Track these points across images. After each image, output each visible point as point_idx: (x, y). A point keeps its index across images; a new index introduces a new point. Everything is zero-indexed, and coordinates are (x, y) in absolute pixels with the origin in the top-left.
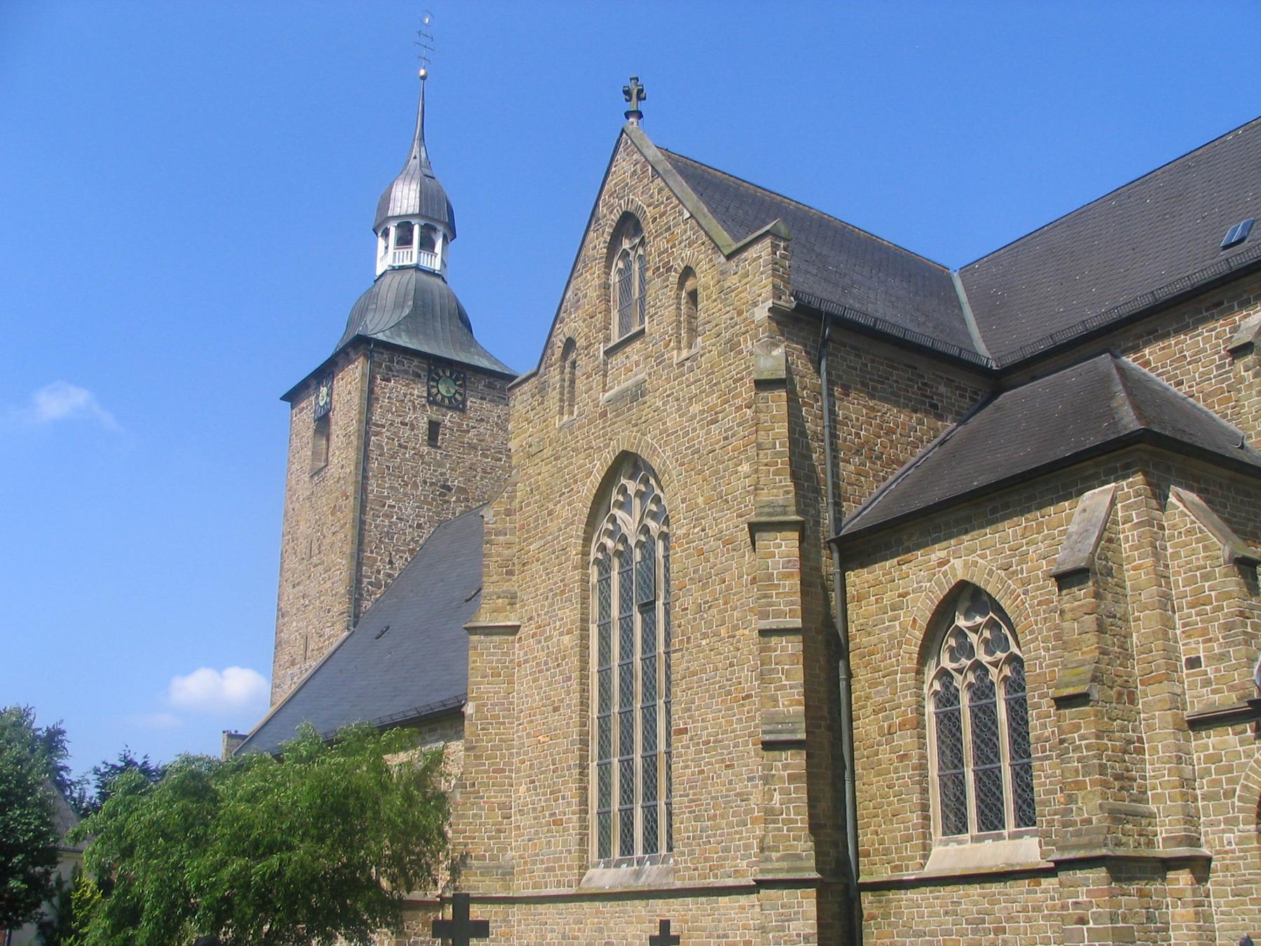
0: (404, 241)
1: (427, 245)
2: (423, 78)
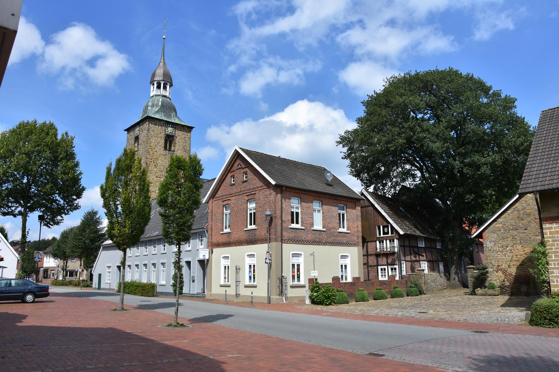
0: (159, 87)
1: (165, 88)
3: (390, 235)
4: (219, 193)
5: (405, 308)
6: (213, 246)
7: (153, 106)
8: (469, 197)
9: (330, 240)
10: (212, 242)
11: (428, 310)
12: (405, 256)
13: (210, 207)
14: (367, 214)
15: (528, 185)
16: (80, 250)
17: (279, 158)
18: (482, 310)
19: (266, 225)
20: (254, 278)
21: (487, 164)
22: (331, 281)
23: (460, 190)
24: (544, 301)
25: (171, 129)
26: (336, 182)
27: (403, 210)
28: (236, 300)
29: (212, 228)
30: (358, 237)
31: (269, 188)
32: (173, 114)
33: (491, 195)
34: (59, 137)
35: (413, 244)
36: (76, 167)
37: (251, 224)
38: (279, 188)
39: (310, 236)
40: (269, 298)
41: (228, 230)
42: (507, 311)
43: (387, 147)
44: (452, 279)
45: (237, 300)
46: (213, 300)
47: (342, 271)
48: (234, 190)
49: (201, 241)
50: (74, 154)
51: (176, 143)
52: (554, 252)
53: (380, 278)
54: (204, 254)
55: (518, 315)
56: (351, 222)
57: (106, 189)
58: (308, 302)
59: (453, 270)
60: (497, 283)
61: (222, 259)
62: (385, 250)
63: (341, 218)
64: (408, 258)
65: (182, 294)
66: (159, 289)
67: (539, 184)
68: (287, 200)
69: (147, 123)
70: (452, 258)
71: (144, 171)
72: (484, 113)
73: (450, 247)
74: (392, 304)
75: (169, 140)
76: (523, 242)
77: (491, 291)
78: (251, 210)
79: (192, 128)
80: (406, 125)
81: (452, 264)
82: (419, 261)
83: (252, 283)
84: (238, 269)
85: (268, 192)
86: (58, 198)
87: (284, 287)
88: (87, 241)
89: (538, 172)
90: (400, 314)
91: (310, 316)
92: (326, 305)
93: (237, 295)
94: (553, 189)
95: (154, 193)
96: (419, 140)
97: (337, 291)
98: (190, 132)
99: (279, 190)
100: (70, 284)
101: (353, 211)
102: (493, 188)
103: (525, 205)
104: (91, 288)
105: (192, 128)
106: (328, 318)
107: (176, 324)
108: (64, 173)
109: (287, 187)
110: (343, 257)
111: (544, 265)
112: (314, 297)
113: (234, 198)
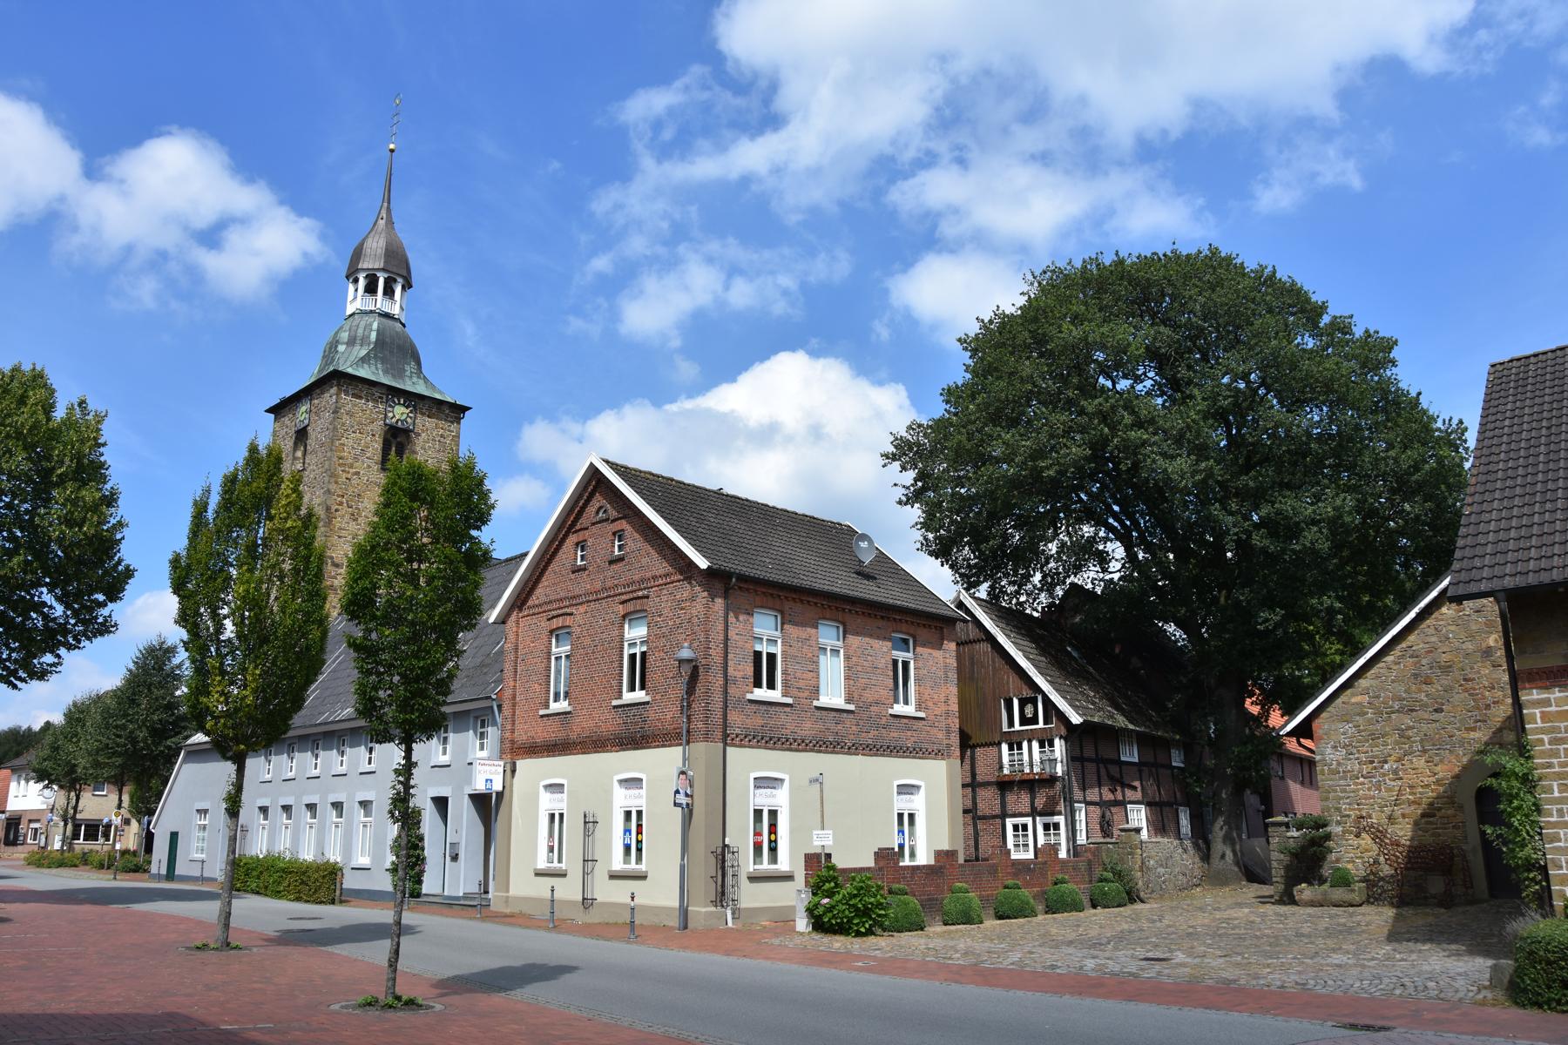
0: (371, 289)
1: (389, 292)
2: (392, 151)
3: (1041, 725)
5: (1097, 945)
6: (515, 751)
7: (351, 342)
8: (1269, 618)
9: (868, 738)
10: (513, 742)
11: (1171, 951)
12: (1084, 789)
13: (511, 637)
14: (972, 664)
15: (1475, 574)
16: (118, 761)
17: (719, 493)
18: (1334, 950)
19: (679, 690)
20: (639, 850)
21: (1319, 521)
22: (870, 863)
23: (1243, 596)
24: (1531, 926)
25: (403, 409)
26: (886, 567)
27: (1075, 654)
28: (581, 918)
29: (514, 697)
30: (948, 732)
31: (688, 579)
32: (410, 368)
33: (1331, 611)
34: (60, 413)
35: (1107, 753)
36: (109, 505)
37: (632, 688)
38: (718, 580)
39: (808, 725)
40: (684, 913)
41: (563, 705)
42: (1414, 956)
43: (1035, 468)
44: (1215, 856)
45: (587, 918)
46: (512, 916)
47: (901, 832)
48: (584, 584)
49: (482, 736)
50: (102, 465)
52: (1558, 774)
53: (1014, 856)
54: (488, 775)
55: (1456, 971)
56: (928, 685)
57: (189, 566)
58: (802, 924)
59: (1218, 829)
60: (1357, 869)
61: (543, 791)
62: (1027, 770)
63: (899, 673)
64: (1093, 795)
65: (419, 895)
66: (350, 882)
67: (1508, 569)
68: (741, 618)
69: (334, 390)
70: (1216, 794)
71: (310, 515)
72: (1309, 375)
73: (1210, 763)
74: (1054, 931)
75: (396, 438)
76: (1431, 747)
77: (1339, 894)
78: (632, 645)
79: (464, 409)
80: (1090, 406)
81: (1217, 812)
82: (1122, 804)
83: (633, 866)
84: (589, 823)
85: (685, 590)
86: (48, 598)
87: (729, 879)
88: (142, 734)
89: (1502, 535)
90: (1090, 964)
91: (814, 970)
92: (858, 934)
93: (587, 902)
94: (1554, 585)
95: (337, 580)
96: (1133, 449)
97: (890, 892)
98: (458, 420)
99: (719, 586)
100: (85, 860)
101: (937, 654)
102: (1335, 591)
103: (1433, 639)
104: (146, 876)
105: (464, 409)
106: (872, 977)
107: (390, 1000)
108: (69, 521)
109: (743, 578)
110: (906, 789)
111: (1527, 816)
112: (821, 910)
113: (582, 609)
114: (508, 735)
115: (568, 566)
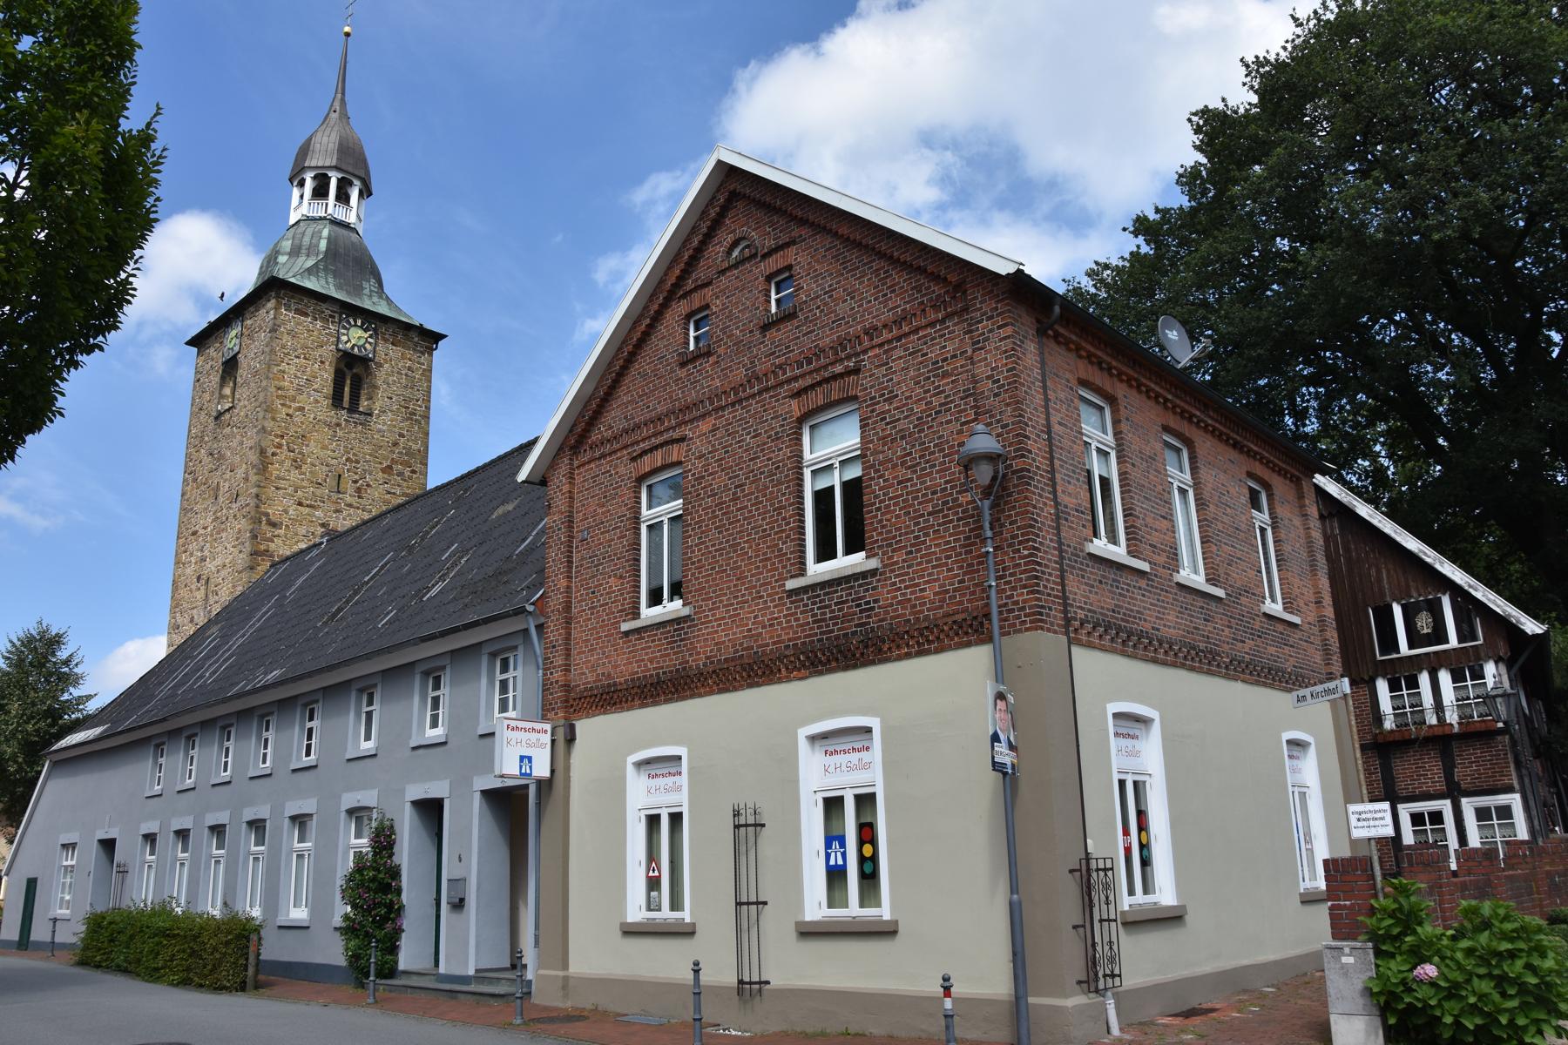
0: (320, 192)
1: (343, 197)
2: (348, 35)
3: (1453, 641)
4: (615, 419)
6: (568, 705)
7: (295, 252)
9: (1245, 649)
10: (567, 687)
13: (560, 502)
25: (360, 333)
37: (826, 551)
41: (673, 607)
48: (709, 378)
51: (376, 387)
54: (522, 749)
61: (637, 774)
62: (1432, 720)
69: (271, 304)
75: (352, 375)
83: (853, 909)
84: (746, 827)
93: (749, 990)
98: (430, 351)
105: (444, 336)
113: (704, 426)
114: (557, 675)
115: (673, 358)
